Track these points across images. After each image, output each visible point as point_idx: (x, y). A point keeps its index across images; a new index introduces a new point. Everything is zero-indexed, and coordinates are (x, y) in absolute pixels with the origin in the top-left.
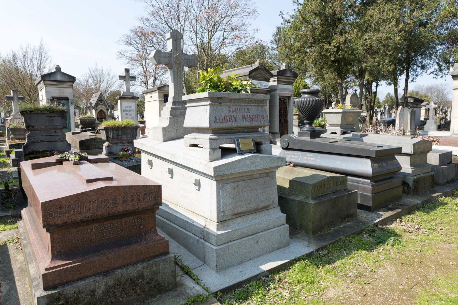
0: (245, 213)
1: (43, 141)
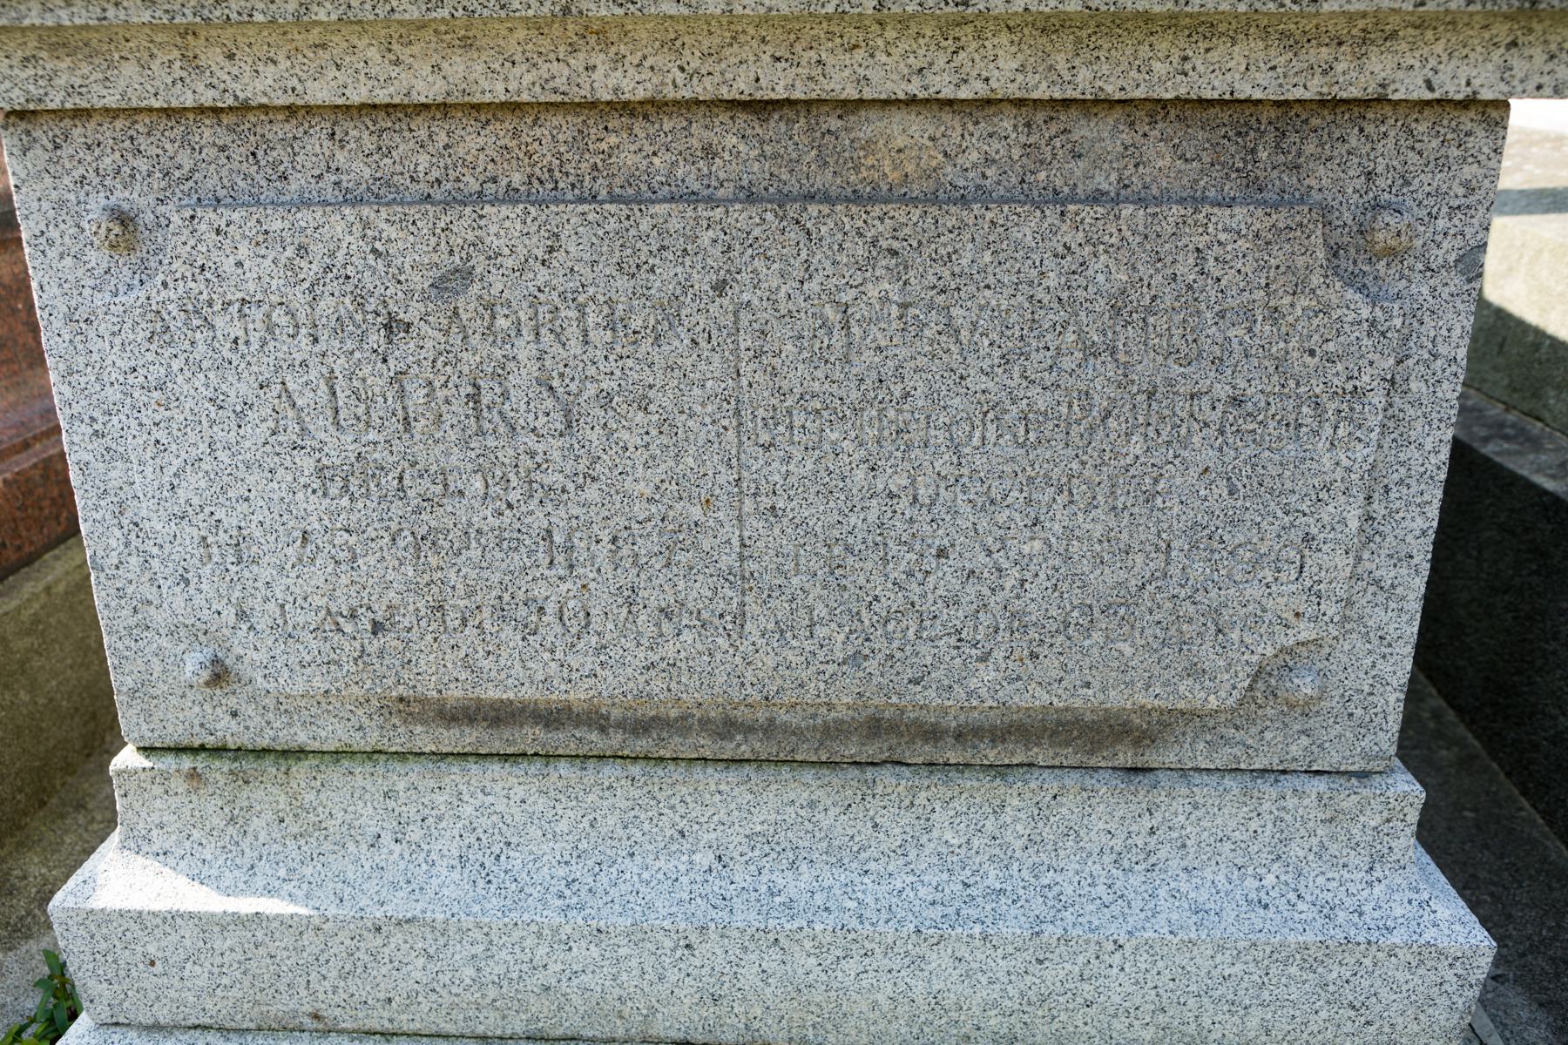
0: (641, 727)
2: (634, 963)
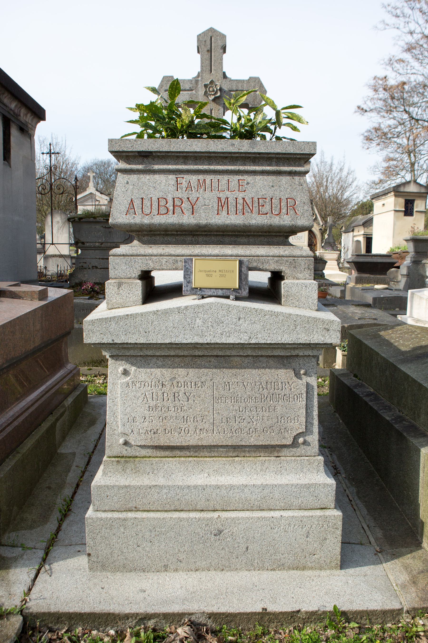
1: (96, 267)
2: (194, 493)
